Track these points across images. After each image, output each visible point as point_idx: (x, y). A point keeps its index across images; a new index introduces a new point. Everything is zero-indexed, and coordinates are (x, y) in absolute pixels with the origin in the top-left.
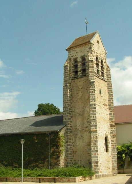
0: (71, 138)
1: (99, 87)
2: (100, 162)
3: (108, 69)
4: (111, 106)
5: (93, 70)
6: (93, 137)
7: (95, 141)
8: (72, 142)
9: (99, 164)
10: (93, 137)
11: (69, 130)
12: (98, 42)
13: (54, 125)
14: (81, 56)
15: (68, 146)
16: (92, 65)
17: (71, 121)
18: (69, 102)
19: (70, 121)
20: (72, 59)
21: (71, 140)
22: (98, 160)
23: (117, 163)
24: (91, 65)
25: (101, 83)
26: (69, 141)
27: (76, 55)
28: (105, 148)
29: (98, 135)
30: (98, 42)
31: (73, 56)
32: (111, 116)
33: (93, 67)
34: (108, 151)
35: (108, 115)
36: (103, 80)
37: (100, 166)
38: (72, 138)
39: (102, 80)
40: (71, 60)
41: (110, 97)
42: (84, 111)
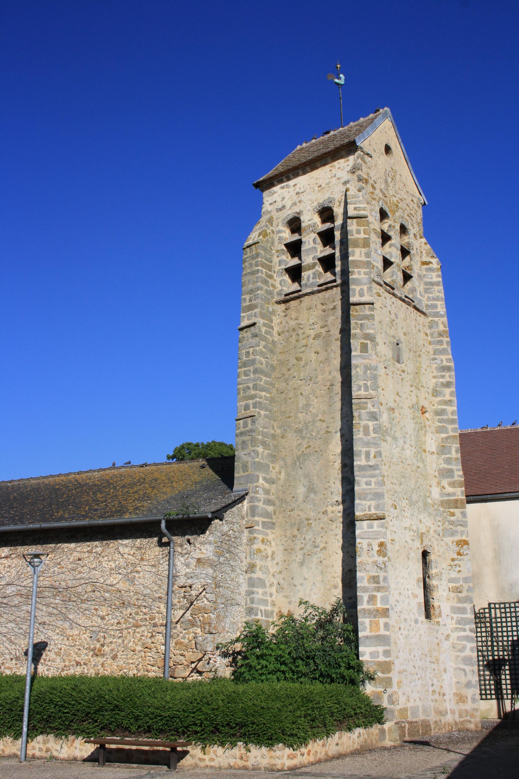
0: (270, 554)
1: (392, 332)
2: (397, 667)
3: (430, 262)
4: (445, 417)
5: (368, 255)
6: (365, 546)
7: (375, 563)
8: (272, 570)
9: (394, 676)
10: (365, 546)
11: (262, 516)
12: (388, 149)
13: (328, 255)
14: (315, 204)
15: (255, 589)
16: (362, 236)
17: (268, 477)
18: (198, 456)
19: (265, 479)
20: (280, 220)
21: (269, 563)
22: (387, 653)
23: (357, 545)
24: (358, 236)
25: (401, 315)
26: (259, 563)
27: (295, 204)
28: (421, 599)
29: (389, 537)
30: (388, 149)
31: (284, 207)
32: (448, 461)
33: (366, 243)
34: (437, 612)
35: (433, 453)
36: (409, 304)
37: (399, 683)
38: (273, 553)
39: (405, 305)
40: (275, 223)
41: (443, 377)
42: (328, 432)
